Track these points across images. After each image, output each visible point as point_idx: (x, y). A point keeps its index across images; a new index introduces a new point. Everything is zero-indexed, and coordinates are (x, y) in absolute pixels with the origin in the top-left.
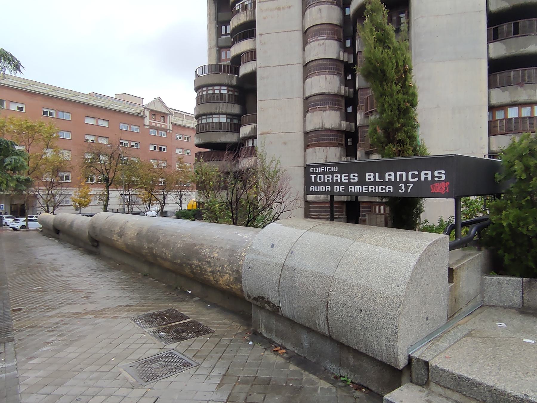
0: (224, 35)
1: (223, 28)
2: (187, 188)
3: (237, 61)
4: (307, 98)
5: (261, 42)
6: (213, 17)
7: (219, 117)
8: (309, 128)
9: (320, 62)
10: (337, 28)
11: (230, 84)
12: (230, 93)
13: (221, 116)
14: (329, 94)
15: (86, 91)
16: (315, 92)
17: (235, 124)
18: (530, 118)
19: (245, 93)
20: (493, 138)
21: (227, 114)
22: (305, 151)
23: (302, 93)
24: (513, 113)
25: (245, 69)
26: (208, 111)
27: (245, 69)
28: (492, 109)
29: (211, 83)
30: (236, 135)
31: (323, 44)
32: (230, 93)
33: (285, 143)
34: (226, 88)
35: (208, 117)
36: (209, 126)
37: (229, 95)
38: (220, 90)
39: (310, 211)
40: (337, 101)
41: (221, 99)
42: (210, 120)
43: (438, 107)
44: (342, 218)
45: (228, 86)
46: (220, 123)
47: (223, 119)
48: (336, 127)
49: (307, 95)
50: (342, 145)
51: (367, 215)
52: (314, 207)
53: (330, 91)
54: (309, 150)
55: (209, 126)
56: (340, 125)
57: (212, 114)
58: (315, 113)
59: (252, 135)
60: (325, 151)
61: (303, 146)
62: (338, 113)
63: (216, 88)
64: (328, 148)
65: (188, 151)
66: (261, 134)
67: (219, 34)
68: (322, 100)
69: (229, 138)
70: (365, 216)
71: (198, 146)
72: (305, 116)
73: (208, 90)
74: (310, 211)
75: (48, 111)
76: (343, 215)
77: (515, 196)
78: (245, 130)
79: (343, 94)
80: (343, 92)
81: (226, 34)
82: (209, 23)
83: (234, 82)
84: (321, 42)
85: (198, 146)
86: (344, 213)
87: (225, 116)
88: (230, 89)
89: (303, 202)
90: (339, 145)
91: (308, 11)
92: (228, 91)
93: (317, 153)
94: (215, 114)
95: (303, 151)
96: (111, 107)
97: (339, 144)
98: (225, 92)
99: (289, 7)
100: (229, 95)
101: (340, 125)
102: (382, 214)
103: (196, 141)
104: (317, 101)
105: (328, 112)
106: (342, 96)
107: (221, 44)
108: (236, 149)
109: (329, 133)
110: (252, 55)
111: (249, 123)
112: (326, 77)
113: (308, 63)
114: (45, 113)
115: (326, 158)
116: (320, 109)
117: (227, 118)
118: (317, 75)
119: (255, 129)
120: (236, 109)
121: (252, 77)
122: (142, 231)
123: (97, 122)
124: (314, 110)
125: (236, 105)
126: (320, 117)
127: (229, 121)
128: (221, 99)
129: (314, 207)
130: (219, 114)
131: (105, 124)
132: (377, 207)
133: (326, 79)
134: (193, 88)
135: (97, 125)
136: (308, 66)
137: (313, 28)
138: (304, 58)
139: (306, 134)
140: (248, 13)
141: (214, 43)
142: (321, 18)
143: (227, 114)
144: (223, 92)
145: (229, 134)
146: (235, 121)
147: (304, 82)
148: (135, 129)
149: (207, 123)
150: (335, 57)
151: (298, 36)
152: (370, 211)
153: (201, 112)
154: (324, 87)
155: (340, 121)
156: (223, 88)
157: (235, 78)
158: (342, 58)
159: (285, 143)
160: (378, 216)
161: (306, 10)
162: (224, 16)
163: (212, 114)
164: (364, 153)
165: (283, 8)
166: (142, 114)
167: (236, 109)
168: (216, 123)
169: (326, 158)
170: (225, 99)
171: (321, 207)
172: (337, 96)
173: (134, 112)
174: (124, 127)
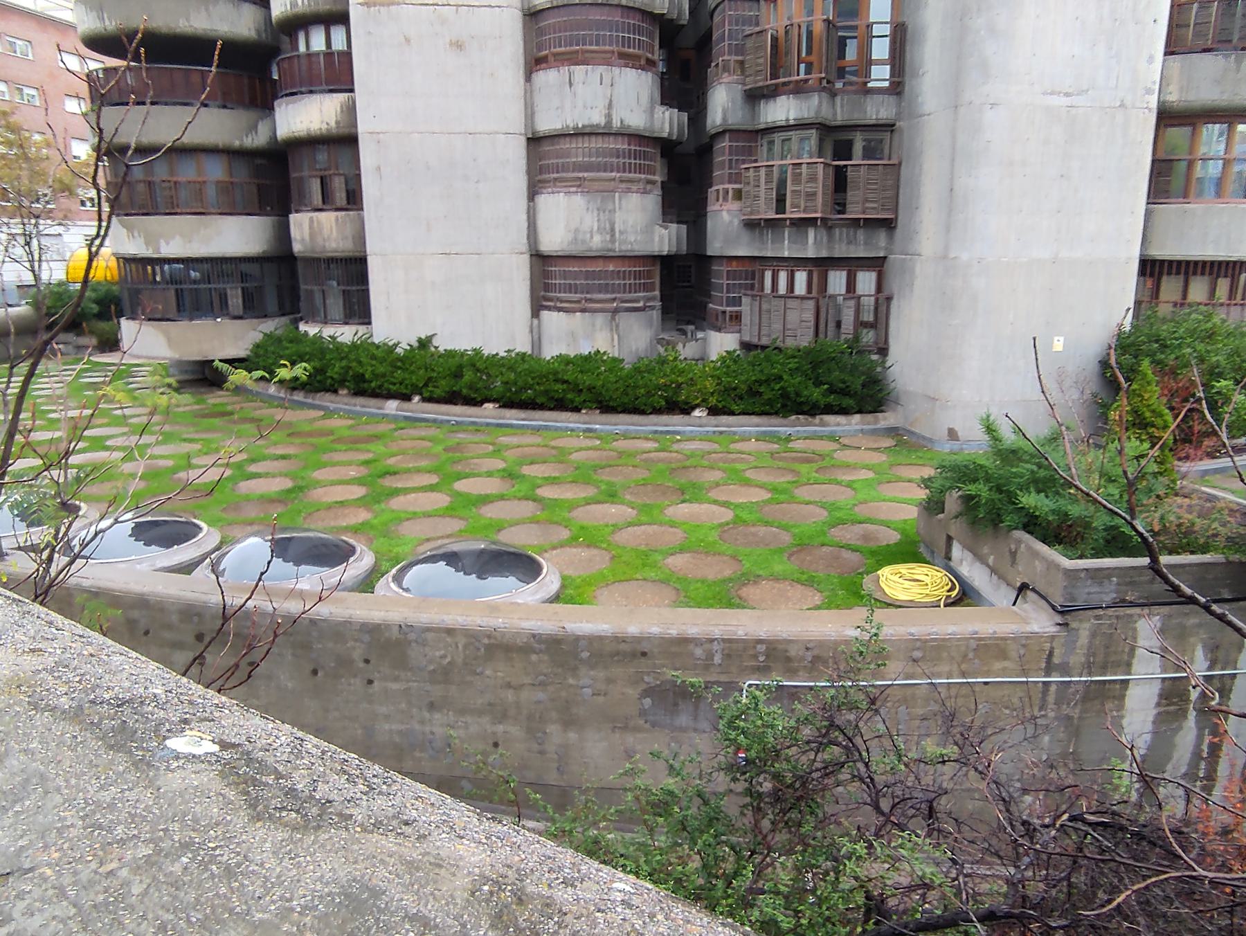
2: (49, 214)
20: (1176, 61)
22: (528, 78)
33: (458, 45)
39: (547, 287)
44: (652, 308)
51: (744, 300)
52: (565, 275)
54: (548, 78)
60: (607, 80)
64: (616, 70)
65: (27, 91)
74: (547, 287)
76: (653, 299)
85: (98, 43)
89: (526, 257)
93: (579, 87)
95: (522, 81)
102: (802, 298)
115: (610, 106)
122: (577, 230)
129: (565, 275)
152: (752, 287)
159: (458, 45)
160: (791, 303)
164: (739, 97)
169: (610, 106)
171: (588, 275)
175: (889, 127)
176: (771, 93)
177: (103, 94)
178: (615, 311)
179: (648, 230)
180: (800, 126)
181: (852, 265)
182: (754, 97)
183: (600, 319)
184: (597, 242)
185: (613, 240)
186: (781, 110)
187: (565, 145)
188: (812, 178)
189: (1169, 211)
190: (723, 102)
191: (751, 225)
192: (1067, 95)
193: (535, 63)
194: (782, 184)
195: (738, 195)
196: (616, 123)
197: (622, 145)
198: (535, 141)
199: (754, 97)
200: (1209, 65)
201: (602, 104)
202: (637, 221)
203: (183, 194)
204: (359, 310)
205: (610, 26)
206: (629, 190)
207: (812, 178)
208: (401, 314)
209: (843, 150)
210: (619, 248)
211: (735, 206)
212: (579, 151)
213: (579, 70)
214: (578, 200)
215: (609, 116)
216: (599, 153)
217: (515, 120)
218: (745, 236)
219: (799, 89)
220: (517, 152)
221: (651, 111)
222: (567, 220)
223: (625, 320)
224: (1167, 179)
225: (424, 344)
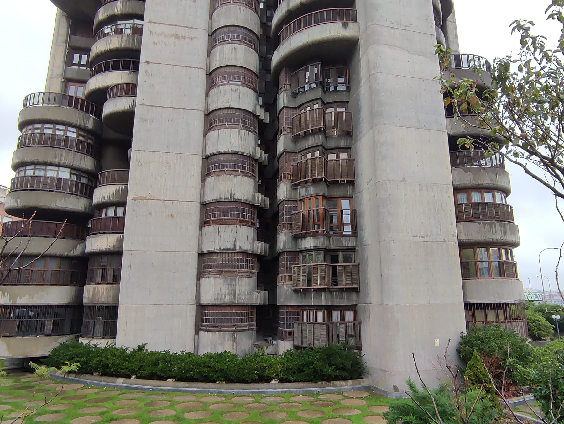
0: (75, 65)
1: (76, 57)
3: (99, 97)
4: (207, 158)
5: (146, 72)
6: (62, 38)
7: (58, 171)
8: (209, 198)
9: (232, 112)
10: (254, 76)
11: (83, 125)
12: (81, 138)
13: (61, 169)
14: (242, 155)
16: (222, 148)
17: (83, 184)
18: (493, 204)
19: (109, 141)
21: (72, 168)
22: (201, 229)
23: (201, 150)
24: (476, 197)
25: (111, 107)
26: (41, 159)
27: (111, 107)
28: (457, 190)
29: (52, 118)
31: (237, 90)
32: (81, 138)
33: (172, 216)
35: (38, 167)
37: (79, 141)
38: (65, 131)
40: (251, 165)
41: (66, 145)
42: (40, 173)
43: (404, 180)
45: (79, 128)
46: (59, 180)
47: (65, 174)
48: (249, 199)
49: (208, 153)
52: (212, 314)
53: (243, 151)
54: (208, 229)
56: (254, 197)
57: (46, 164)
58: (221, 177)
59: (115, 200)
60: (234, 230)
63: (58, 127)
64: (238, 227)
66: (134, 199)
67: (69, 62)
69: (77, 204)
70: (291, 326)
71: (11, 212)
72: (203, 181)
76: (253, 325)
78: (102, 194)
79: (258, 158)
80: (259, 155)
81: (79, 65)
82: (55, 44)
83: (90, 125)
84: (235, 87)
85: (11, 212)
86: (255, 322)
87: (69, 170)
88: (80, 132)
91: (218, 48)
92: (79, 135)
93: (222, 234)
94: (51, 164)
95: (198, 230)
98: (74, 135)
99: (192, 38)
100: (79, 141)
101: (254, 197)
102: (321, 324)
103: (10, 203)
104: (224, 161)
105: (239, 178)
106: (256, 161)
107: (69, 75)
108: (80, 224)
109: (239, 207)
110: (130, 89)
111: (113, 182)
112: (239, 131)
113: (212, 155)
116: (229, 173)
117: (71, 174)
118: (226, 128)
119: (125, 192)
120: (88, 163)
121: (126, 120)
124: (218, 173)
125: (89, 157)
126: (229, 183)
127: (74, 178)
129: (212, 314)
130: (59, 165)
132: (312, 314)
133: (239, 134)
134: (16, 121)
136: (212, 115)
137: (223, 69)
138: (207, 105)
139: (204, 205)
140: (124, 38)
141: (59, 70)
142: (236, 58)
143: (72, 168)
144: (69, 134)
145: (72, 199)
146: (84, 180)
147: (205, 136)
149: (34, 177)
150: (251, 110)
151: (202, 77)
152: (298, 319)
153: (28, 159)
154: (235, 145)
155: (254, 192)
156: (70, 129)
157: (91, 119)
158: (258, 114)
159: (172, 216)
160: (315, 326)
161: (214, 47)
162: (80, 41)
163: (46, 164)
164: (290, 238)
165: (183, 37)
167: (88, 163)
168: (52, 179)
172: (251, 158)
175: (353, 250)
176: (304, 236)
178: (235, 331)
179: (251, 293)
180: (316, 249)
182: (296, 238)
184: (227, 299)
185: (234, 299)
186: (308, 243)
187: (215, 257)
189: (471, 282)
190: (283, 240)
191: (296, 291)
192: (422, 237)
193: (206, 174)
194: (309, 273)
195: (291, 278)
196: (238, 248)
197: (240, 257)
198: (202, 255)
199: (296, 238)
202: (246, 290)
205: (238, 261)
206: (243, 276)
209: (335, 259)
211: (290, 283)
212: (221, 260)
213: (222, 227)
214: (220, 281)
215: (235, 245)
217: (194, 248)
218: (294, 296)
219: (315, 235)
220: (193, 260)
222: (214, 290)
223: (239, 335)
224: (468, 270)
225: (141, 348)
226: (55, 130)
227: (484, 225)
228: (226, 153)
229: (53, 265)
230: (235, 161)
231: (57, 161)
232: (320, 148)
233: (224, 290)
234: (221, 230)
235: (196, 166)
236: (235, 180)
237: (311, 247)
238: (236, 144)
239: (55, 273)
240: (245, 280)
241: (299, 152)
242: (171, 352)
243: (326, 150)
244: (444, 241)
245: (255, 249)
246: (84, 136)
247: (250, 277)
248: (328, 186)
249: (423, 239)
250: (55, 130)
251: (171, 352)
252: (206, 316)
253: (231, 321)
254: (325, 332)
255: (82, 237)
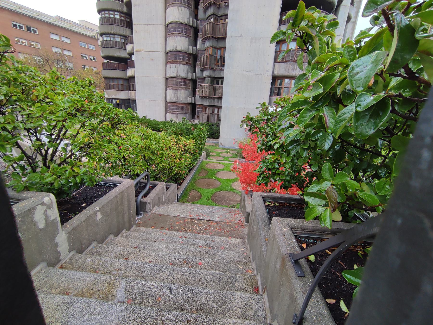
4: (168, 53)
8: (168, 49)
11: (121, 11)
12: (122, 18)
14: (180, 23)
15: (76, 20)
20: (277, 65)
30: (123, 51)
32: (122, 18)
33: (152, 59)
34: (118, 14)
36: (108, 43)
37: (121, 20)
38: (114, 15)
40: (186, 29)
43: (241, 36)
46: (116, 42)
50: (190, 64)
53: (181, 21)
55: (108, 43)
56: (188, 48)
61: (164, 62)
62: (187, 39)
68: (175, 28)
71: (105, 57)
73: (105, 14)
75: (18, 24)
77: (25, 228)
78: (129, 47)
79: (191, 25)
87: (119, 37)
90: (187, 64)
92: (121, 16)
93: (172, 68)
96: (71, 29)
97: (187, 63)
105: (179, 37)
112: (178, 8)
114: (15, 26)
115: (177, 72)
119: (133, 47)
123: (60, 38)
125: (127, 29)
126: (174, 41)
127: (123, 41)
128: (115, 23)
130: (114, 34)
131: (68, 41)
133: (178, 10)
135: (61, 41)
139: (167, 53)
144: (116, 16)
148: (91, 47)
156: (116, 13)
159: (152, 59)
163: (114, 34)
166: (96, 37)
170: (118, 23)
171: (173, 106)
172: (186, 25)
173: (90, 35)
174: (83, 45)
177: (105, 67)
178: (177, 114)
179: (186, 98)
180: (207, 77)
181: (213, 107)
183: (174, 115)
185: (177, 99)
186: (206, 74)
188: (207, 88)
191: (202, 98)
192: (247, 71)
193: (167, 62)
196: (178, 76)
197: (180, 80)
198: (167, 79)
200: (283, 66)
201: (176, 72)
202: (183, 95)
203: (115, 87)
204: (135, 109)
206: (181, 89)
207: (207, 88)
208: (141, 111)
210: (178, 101)
215: (177, 74)
216: (177, 82)
218: (200, 100)
220: (163, 81)
221: (188, 73)
222: (171, 95)
223: (179, 115)
225: (145, 117)
226: (110, 14)
227: (289, 65)
228: (172, 23)
229: (121, 82)
230: (177, 28)
231: (112, 32)
232: (213, 16)
233: (173, 95)
234: (172, 66)
235: (161, 30)
236: (177, 39)
237: (177, 75)
238: (177, 17)
239: (123, 86)
240: (182, 92)
241: (207, 19)
242: (147, 118)
243: (219, 17)
244: (261, 74)
245: (189, 76)
246: (123, 17)
247: (185, 90)
248: (217, 41)
249: (248, 73)
250: (110, 14)
251: (147, 118)
252: (169, 106)
253: (176, 109)
254: (206, 117)
255: (125, 70)
